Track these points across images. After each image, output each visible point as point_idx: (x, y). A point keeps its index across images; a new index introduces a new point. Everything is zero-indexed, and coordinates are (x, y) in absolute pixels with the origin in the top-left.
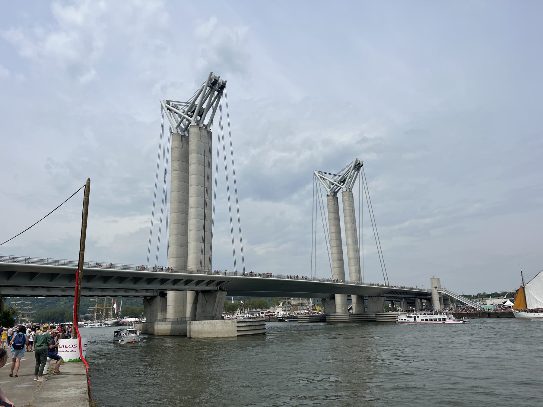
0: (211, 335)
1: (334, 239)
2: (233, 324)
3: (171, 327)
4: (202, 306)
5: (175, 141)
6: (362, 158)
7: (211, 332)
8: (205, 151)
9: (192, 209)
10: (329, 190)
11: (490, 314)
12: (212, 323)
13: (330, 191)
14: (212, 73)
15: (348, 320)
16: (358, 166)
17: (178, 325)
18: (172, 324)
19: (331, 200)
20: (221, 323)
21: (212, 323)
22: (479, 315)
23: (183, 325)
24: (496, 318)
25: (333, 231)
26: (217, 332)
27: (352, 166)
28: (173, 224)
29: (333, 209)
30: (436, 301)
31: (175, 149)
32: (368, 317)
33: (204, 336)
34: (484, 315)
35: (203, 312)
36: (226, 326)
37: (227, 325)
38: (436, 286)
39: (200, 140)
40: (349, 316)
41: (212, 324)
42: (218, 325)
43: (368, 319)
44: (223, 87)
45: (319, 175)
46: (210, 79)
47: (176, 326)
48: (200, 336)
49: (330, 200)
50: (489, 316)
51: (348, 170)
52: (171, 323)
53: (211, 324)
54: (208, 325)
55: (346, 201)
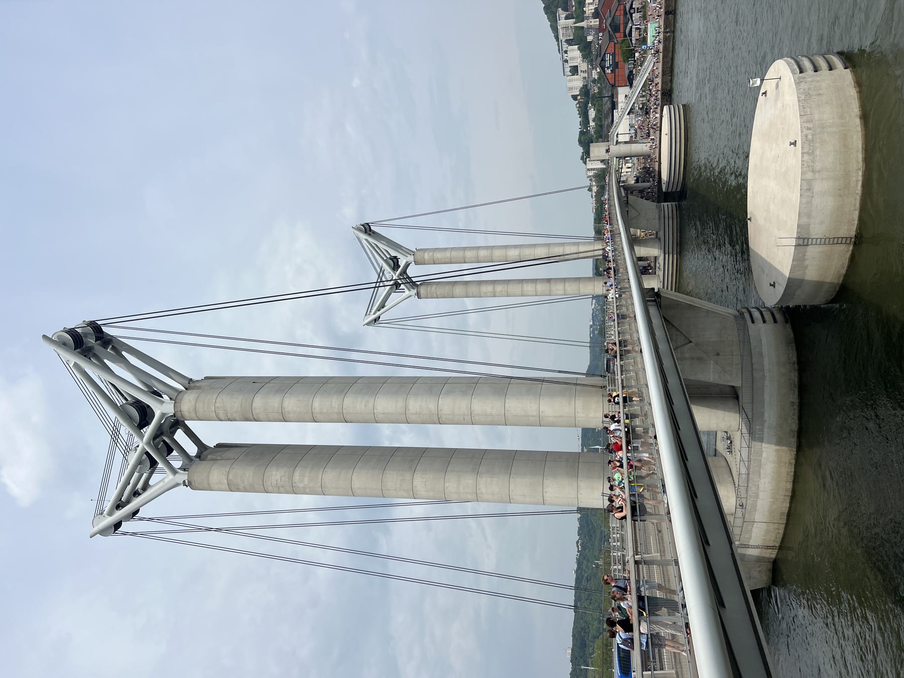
0: (855, 137)
1: (506, 287)
2: (809, 79)
3: (769, 443)
4: (700, 359)
5: (208, 476)
6: (351, 217)
7: (844, 137)
8: (254, 382)
9: (411, 407)
10: (407, 292)
11: (668, 11)
12: (810, 137)
13: (410, 290)
14: (45, 337)
15: (675, 256)
16: (367, 229)
17: (766, 416)
18: (761, 440)
19: (427, 288)
20: (808, 111)
21: (810, 137)
22: (669, 34)
23: (767, 397)
24: (675, 19)
25: (468, 481)
26: (842, 117)
27: (366, 240)
28: (446, 485)
29: (447, 287)
30: (633, 149)
31: (231, 477)
32: (670, 215)
33: (858, 162)
34: (668, 23)
35: (718, 354)
36: (819, 95)
37: (815, 93)
38: (604, 151)
39: (233, 461)
40: (667, 255)
41: (813, 135)
42: (816, 117)
43: (675, 216)
44: (96, 328)
45: (374, 314)
46: (63, 344)
47: (766, 424)
48: (857, 181)
49: (427, 290)
50: (671, 13)
51: (374, 248)
52: (756, 445)
53: (813, 141)
54: (818, 153)
55: (435, 255)
